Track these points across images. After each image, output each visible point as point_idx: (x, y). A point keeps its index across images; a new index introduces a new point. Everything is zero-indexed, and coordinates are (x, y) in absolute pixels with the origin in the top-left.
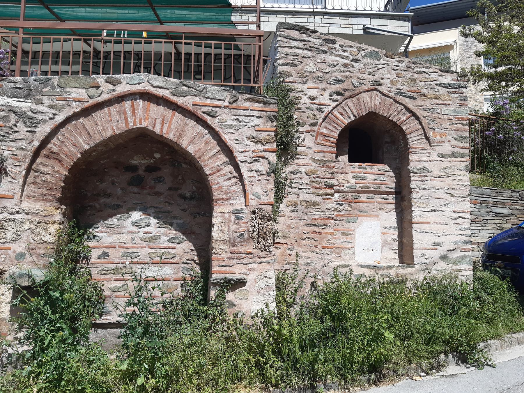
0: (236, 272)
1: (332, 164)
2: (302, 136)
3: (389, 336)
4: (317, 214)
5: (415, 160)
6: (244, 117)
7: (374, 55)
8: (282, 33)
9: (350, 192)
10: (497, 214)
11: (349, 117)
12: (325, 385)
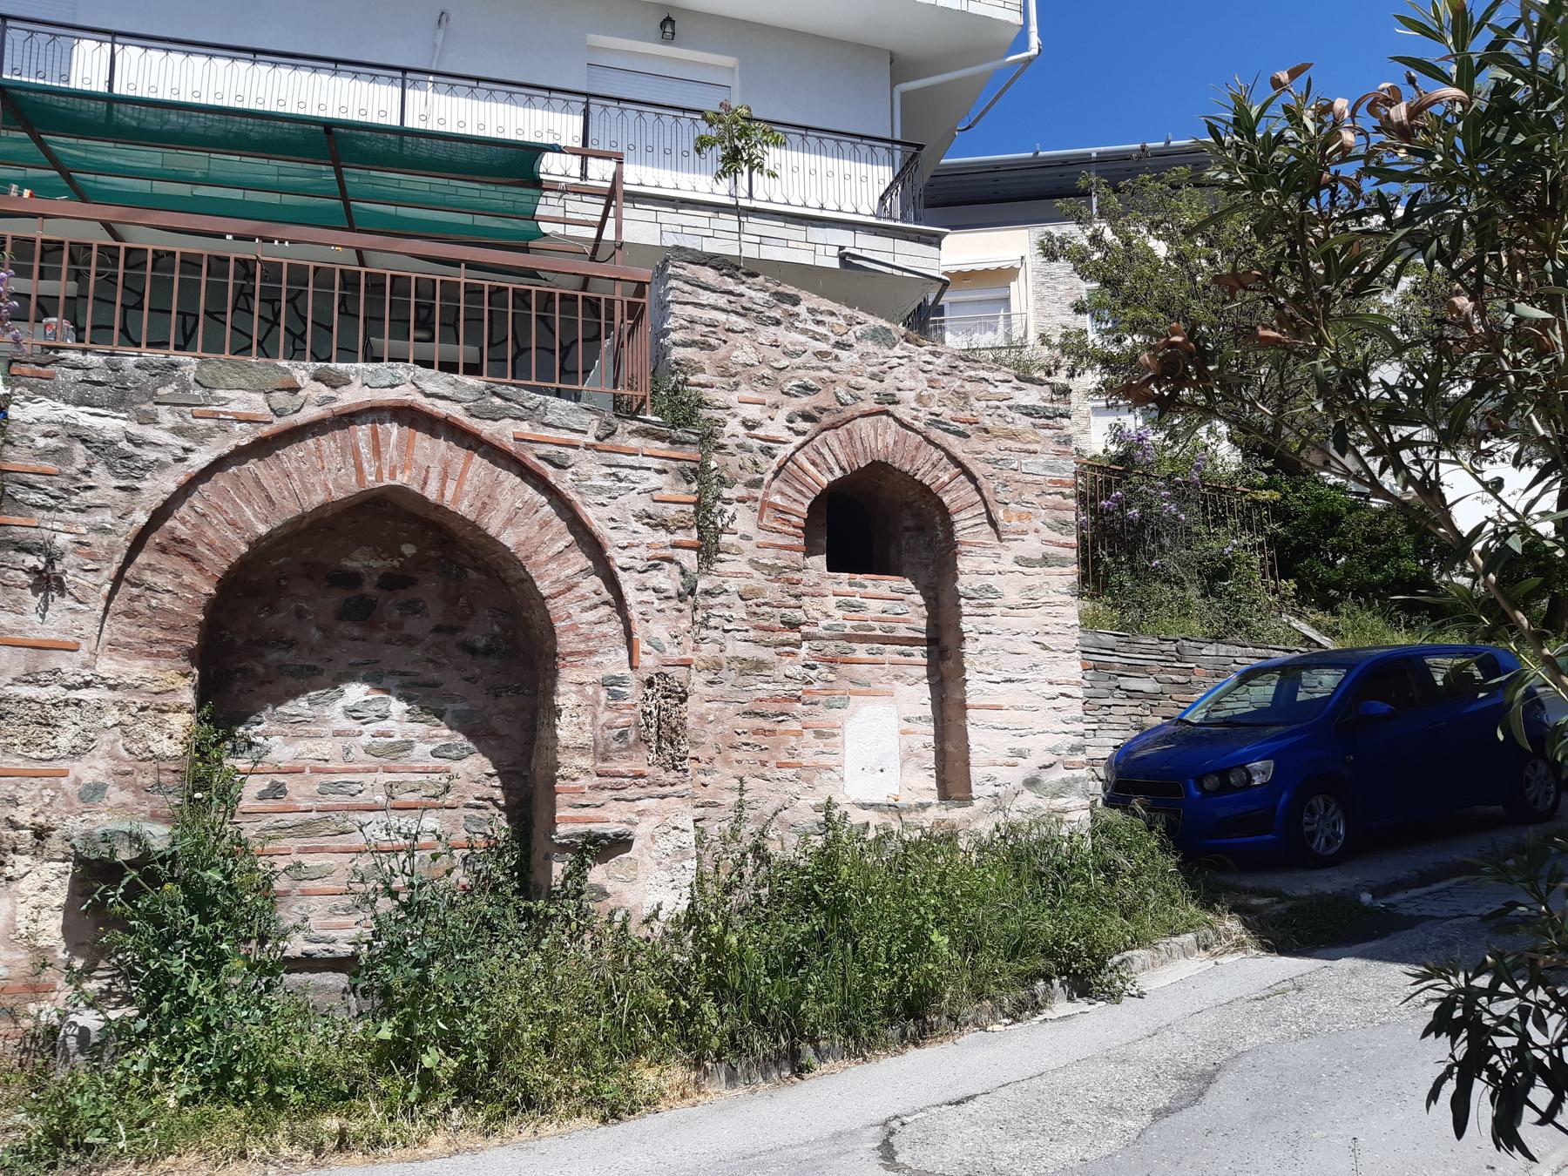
0: (611, 821)
1: (797, 576)
2: (730, 509)
3: (939, 939)
4: (764, 689)
5: (971, 569)
6: (627, 471)
8: (680, 271)
10: (1131, 694)
11: (831, 471)
12: (817, 1050)
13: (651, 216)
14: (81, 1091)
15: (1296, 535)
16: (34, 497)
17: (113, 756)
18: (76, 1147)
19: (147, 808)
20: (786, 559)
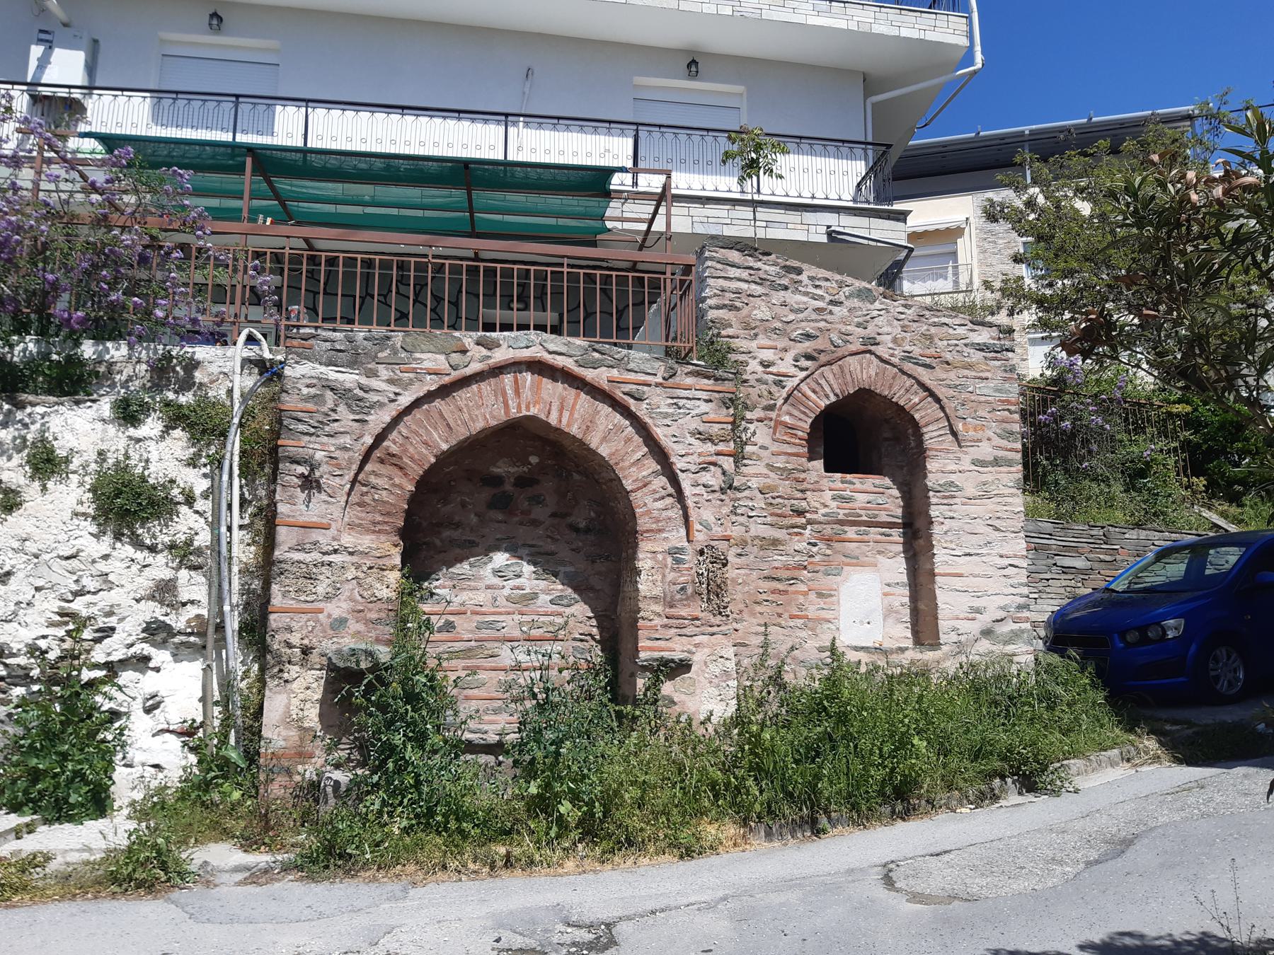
1: (803, 476)
2: (752, 427)
4: (779, 560)
5: (938, 469)
7: (864, 295)
9: (829, 523)
10: (1066, 570)
11: (827, 396)
12: (829, 818)
13: (685, 211)
14: (342, 820)
15: (1205, 441)
16: (301, 427)
17: (352, 599)
18: (341, 856)
19: (373, 634)
20: (794, 463)
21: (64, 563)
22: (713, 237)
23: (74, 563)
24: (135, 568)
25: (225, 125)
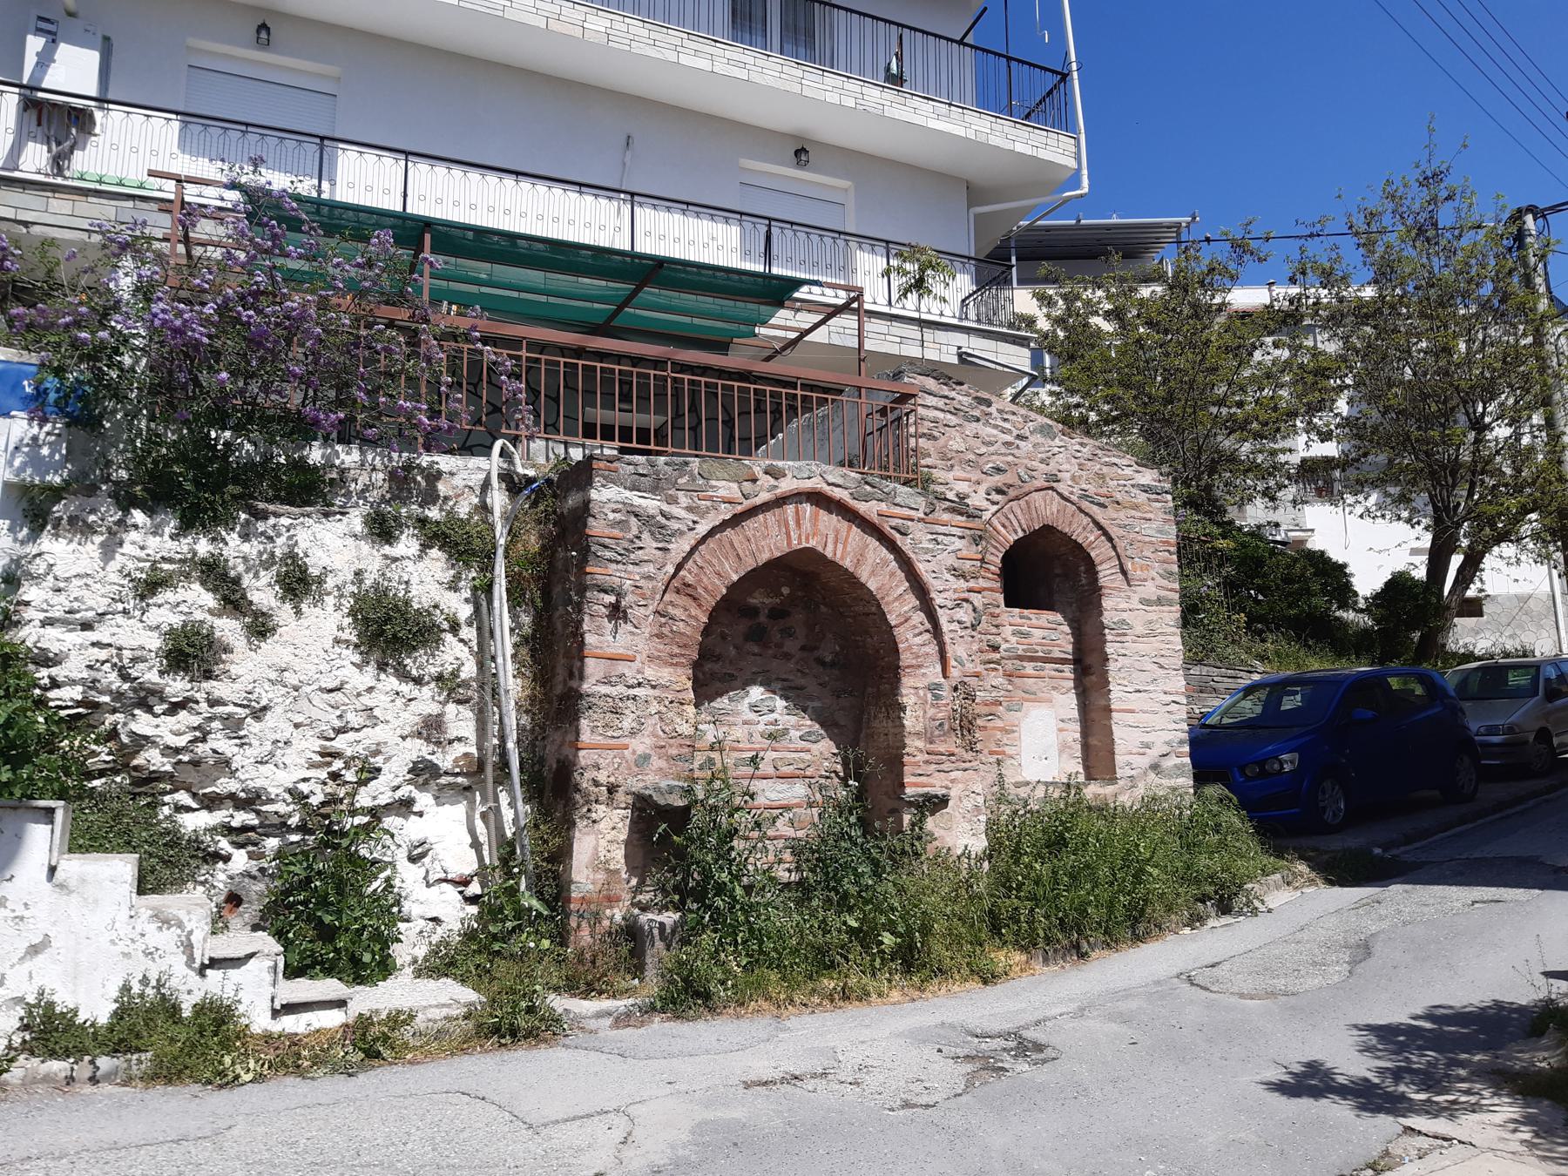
0: (936, 786)
16: (608, 554)
21: (325, 696)
22: (912, 361)
23: (338, 696)
24: (399, 702)
25: (308, 171)
